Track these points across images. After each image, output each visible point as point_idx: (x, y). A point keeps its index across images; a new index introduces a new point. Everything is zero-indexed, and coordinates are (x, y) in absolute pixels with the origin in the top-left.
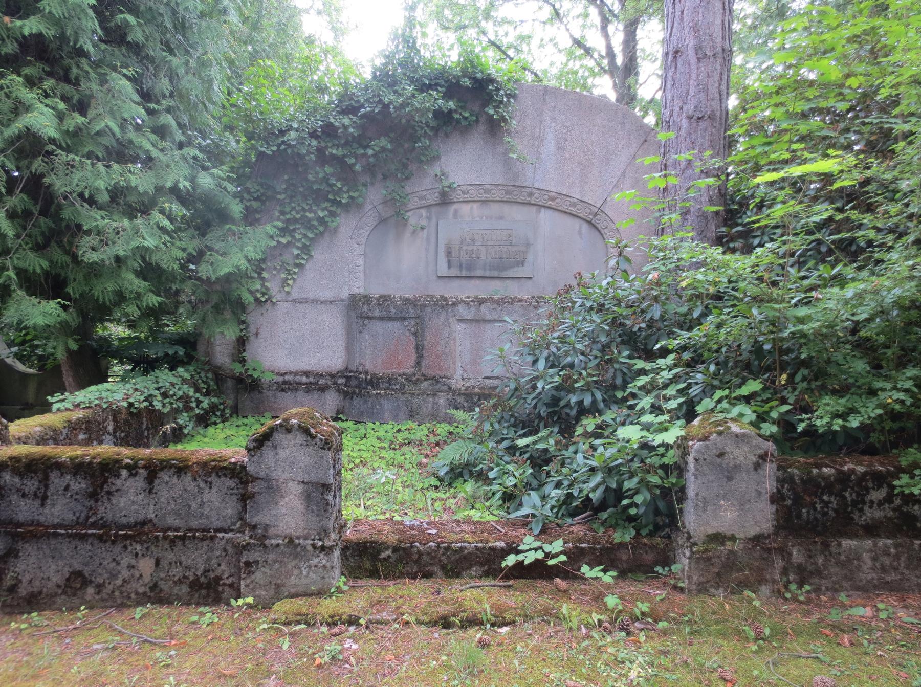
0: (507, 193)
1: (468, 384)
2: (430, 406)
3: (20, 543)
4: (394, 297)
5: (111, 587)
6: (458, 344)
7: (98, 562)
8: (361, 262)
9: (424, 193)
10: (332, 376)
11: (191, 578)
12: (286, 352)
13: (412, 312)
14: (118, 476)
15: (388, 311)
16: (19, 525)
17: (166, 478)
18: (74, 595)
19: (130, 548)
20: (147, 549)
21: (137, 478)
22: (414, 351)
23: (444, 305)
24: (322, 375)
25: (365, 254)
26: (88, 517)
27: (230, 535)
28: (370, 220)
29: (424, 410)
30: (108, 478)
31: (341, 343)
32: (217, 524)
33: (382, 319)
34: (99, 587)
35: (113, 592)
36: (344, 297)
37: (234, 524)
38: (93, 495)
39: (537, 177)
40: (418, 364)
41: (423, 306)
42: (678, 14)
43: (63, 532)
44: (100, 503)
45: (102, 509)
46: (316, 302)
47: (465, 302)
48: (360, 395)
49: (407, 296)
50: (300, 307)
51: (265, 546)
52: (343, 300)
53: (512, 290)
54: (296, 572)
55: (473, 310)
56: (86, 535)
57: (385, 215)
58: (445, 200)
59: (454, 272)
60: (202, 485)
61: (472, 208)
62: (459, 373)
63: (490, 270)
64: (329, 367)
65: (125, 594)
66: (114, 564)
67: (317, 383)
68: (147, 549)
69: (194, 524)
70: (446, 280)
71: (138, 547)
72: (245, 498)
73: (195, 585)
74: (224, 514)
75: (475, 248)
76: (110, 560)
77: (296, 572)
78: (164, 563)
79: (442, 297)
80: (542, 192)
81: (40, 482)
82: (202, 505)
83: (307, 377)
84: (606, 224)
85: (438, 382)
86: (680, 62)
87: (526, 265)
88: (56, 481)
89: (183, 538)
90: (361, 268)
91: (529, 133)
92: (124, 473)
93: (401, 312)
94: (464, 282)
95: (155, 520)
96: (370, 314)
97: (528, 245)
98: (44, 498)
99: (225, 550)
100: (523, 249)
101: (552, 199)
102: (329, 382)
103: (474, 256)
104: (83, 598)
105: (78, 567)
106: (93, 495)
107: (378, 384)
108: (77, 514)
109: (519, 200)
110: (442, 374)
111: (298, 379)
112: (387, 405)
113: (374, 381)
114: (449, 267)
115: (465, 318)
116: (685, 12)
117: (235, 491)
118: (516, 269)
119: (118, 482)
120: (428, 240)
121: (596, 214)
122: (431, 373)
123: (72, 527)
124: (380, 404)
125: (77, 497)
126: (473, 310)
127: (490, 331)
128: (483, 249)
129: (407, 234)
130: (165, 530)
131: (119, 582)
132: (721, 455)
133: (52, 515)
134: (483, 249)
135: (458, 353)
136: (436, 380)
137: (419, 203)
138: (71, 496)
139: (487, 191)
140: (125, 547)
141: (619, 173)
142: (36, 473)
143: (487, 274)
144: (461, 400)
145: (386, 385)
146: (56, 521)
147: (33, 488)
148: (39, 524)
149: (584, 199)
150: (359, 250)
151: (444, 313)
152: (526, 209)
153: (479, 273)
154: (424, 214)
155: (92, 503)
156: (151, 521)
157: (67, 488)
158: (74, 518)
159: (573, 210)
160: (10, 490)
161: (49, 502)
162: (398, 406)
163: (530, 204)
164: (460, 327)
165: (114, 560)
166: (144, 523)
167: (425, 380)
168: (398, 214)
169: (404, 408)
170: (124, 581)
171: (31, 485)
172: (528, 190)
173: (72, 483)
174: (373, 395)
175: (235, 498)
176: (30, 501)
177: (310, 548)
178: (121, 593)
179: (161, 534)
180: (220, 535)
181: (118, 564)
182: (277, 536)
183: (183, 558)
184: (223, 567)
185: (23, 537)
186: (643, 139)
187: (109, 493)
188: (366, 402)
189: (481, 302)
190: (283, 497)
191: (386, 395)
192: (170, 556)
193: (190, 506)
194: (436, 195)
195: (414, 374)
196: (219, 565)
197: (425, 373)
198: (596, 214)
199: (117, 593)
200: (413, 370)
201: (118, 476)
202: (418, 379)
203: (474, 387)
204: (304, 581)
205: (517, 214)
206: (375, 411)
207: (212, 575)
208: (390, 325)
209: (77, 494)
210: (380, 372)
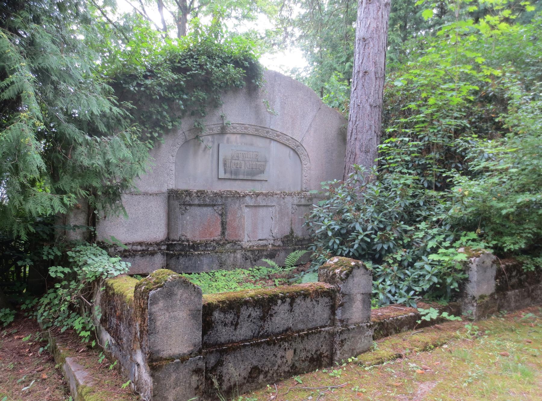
0: (257, 130)
1: (251, 244)
2: (232, 259)
3: (225, 356)
4: (207, 192)
5: (271, 372)
6: (245, 220)
7: (266, 358)
8: (173, 167)
9: (213, 126)
10: (158, 244)
11: (310, 356)
12: (125, 229)
13: (220, 201)
14: (276, 304)
15: (204, 200)
16: (222, 344)
17: (299, 302)
18: (253, 382)
19: (282, 346)
20: (291, 345)
21: (285, 304)
22: (220, 225)
23: (237, 196)
24: (151, 244)
25: (176, 163)
26: (259, 332)
27: (327, 329)
28: (180, 141)
29: (229, 262)
30: (271, 306)
31: (163, 221)
32: (320, 324)
33: (199, 205)
34: (266, 373)
35: (273, 374)
36: (164, 191)
37: (327, 322)
38: (263, 318)
39: (272, 123)
40: (223, 233)
41: (227, 198)
42: (366, 54)
43: (248, 343)
44: (266, 322)
45: (266, 326)
46: (146, 194)
47: (249, 195)
48: (186, 255)
49: (215, 191)
50: (136, 198)
51: (349, 330)
52: (163, 193)
53: (259, 188)
54: (360, 341)
55: (254, 200)
56: (261, 343)
57: (188, 138)
58: (223, 131)
59: (228, 176)
60: (315, 303)
61: (236, 137)
62: (246, 239)
63: (247, 175)
64: (155, 238)
65: (279, 374)
66: (274, 357)
67: (147, 250)
68: (291, 345)
69: (310, 326)
70: (223, 181)
71: (286, 344)
72: (333, 309)
73: (312, 360)
74: (323, 318)
75: (239, 162)
76: (272, 355)
77: (360, 341)
78: (298, 351)
79: (236, 192)
80: (274, 132)
81: (235, 315)
82: (313, 315)
83: (141, 246)
84: (302, 151)
85: (235, 244)
86: (367, 78)
87: (265, 172)
88: (244, 312)
89: (307, 335)
90: (174, 172)
91: (268, 97)
92: (279, 302)
93: (213, 201)
94: (232, 182)
95: (292, 327)
96: (192, 203)
97: (266, 161)
98: (237, 324)
99: (325, 337)
100: (263, 163)
101: (278, 136)
102: (156, 249)
103: (238, 166)
104: (257, 382)
105: (255, 363)
106: (263, 318)
107: (198, 247)
108: (254, 332)
109: (262, 135)
110: (237, 239)
111: (135, 247)
112: (205, 260)
113: (195, 246)
114: (225, 173)
115: (250, 204)
116: (371, 54)
117: (329, 304)
118: (260, 175)
119: (276, 308)
120: (212, 155)
121: (298, 146)
122: (231, 239)
123: (251, 340)
124: (200, 260)
125: (255, 320)
126: (254, 200)
127: (262, 212)
128: (243, 163)
129: (201, 151)
130: (298, 332)
131: (276, 368)
132: (483, 263)
133: (240, 334)
134: (243, 163)
135: (246, 226)
136: (234, 243)
137: (207, 133)
138: (251, 321)
139: (246, 128)
140: (280, 346)
141: (309, 125)
142: (233, 309)
143: (245, 178)
144: (249, 254)
145: (204, 248)
146: (242, 338)
147: (231, 319)
148: (233, 342)
149: (294, 138)
150: (172, 159)
151: (238, 202)
152: (263, 140)
153: (241, 177)
154: (210, 139)
155: (262, 323)
156: (291, 328)
157: (249, 316)
158: (252, 334)
159: (287, 143)
160: (218, 322)
161: (239, 326)
162: (212, 261)
163: (266, 138)
164: (247, 210)
165: (274, 355)
166: (287, 330)
167: (229, 243)
168: (197, 137)
169: (217, 261)
170: (279, 366)
171: (230, 317)
172: (267, 130)
173: (252, 313)
174: (196, 255)
175: (328, 308)
176: (229, 328)
177: (365, 327)
178: (277, 374)
179: (297, 334)
180: (323, 329)
181: (276, 357)
182: (352, 324)
183: (307, 346)
184: (323, 347)
185: (226, 352)
186: (319, 107)
187: (271, 315)
188: (190, 260)
189: (258, 195)
190: (355, 303)
191: (205, 254)
192: (301, 346)
193: (308, 316)
194: (219, 128)
195: (221, 240)
196: (322, 346)
197: (227, 239)
198: (298, 146)
199: (275, 375)
200: (220, 237)
201: (276, 304)
202: (224, 243)
203: (254, 246)
204: (363, 345)
205: (260, 143)
206: (197, 265)
207: (319, 353)
208: (205, 209)
209: (254, 319)
210: (198, 240)
